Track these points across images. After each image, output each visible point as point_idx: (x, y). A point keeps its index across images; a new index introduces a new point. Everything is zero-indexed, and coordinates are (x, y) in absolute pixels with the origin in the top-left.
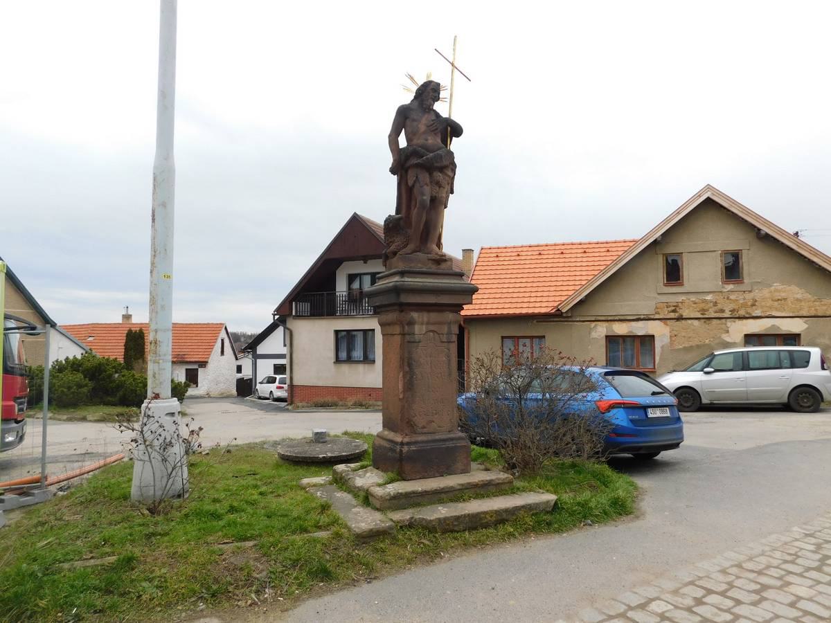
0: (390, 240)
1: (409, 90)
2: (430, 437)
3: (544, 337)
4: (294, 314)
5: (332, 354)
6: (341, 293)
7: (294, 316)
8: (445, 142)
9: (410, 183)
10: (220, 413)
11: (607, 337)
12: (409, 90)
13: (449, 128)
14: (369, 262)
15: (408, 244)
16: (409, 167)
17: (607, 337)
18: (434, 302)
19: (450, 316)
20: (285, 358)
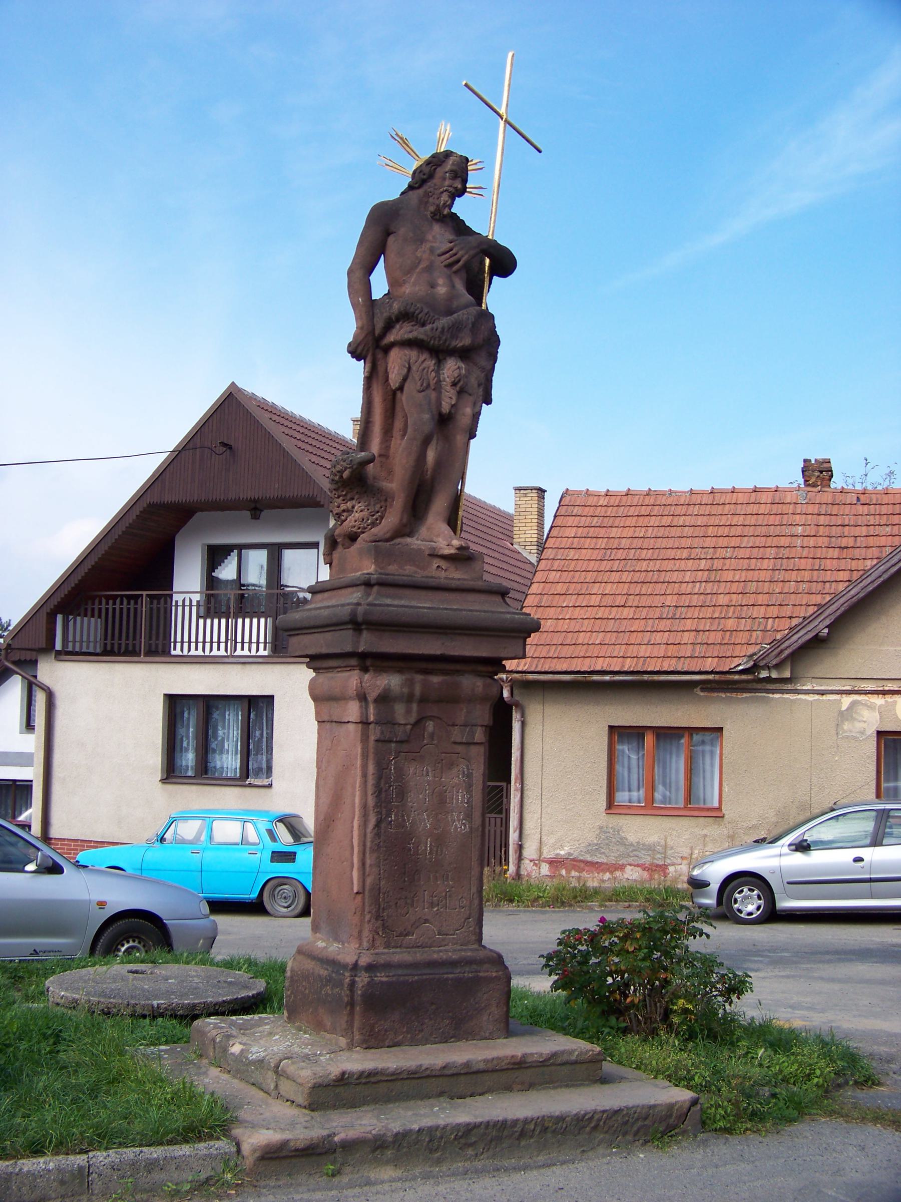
0: (343, 507)
1: (399, 169)
2: (420, 956)
3: (720, 730)
4: (58, 646)
5: (155, 758)
6: (187, 596)
7: (58, 653)
8: (477, 290)
9: (394, 379)
10: (90, 867)
11: (880, 733)
12: (399, 169)
13: (487, 261)
14: (265, 513)
15: (382, 517)
16: (392, 345)
17: (880, 733)
18: (438, 652)
19: (472, 683)
20: (30, 764)
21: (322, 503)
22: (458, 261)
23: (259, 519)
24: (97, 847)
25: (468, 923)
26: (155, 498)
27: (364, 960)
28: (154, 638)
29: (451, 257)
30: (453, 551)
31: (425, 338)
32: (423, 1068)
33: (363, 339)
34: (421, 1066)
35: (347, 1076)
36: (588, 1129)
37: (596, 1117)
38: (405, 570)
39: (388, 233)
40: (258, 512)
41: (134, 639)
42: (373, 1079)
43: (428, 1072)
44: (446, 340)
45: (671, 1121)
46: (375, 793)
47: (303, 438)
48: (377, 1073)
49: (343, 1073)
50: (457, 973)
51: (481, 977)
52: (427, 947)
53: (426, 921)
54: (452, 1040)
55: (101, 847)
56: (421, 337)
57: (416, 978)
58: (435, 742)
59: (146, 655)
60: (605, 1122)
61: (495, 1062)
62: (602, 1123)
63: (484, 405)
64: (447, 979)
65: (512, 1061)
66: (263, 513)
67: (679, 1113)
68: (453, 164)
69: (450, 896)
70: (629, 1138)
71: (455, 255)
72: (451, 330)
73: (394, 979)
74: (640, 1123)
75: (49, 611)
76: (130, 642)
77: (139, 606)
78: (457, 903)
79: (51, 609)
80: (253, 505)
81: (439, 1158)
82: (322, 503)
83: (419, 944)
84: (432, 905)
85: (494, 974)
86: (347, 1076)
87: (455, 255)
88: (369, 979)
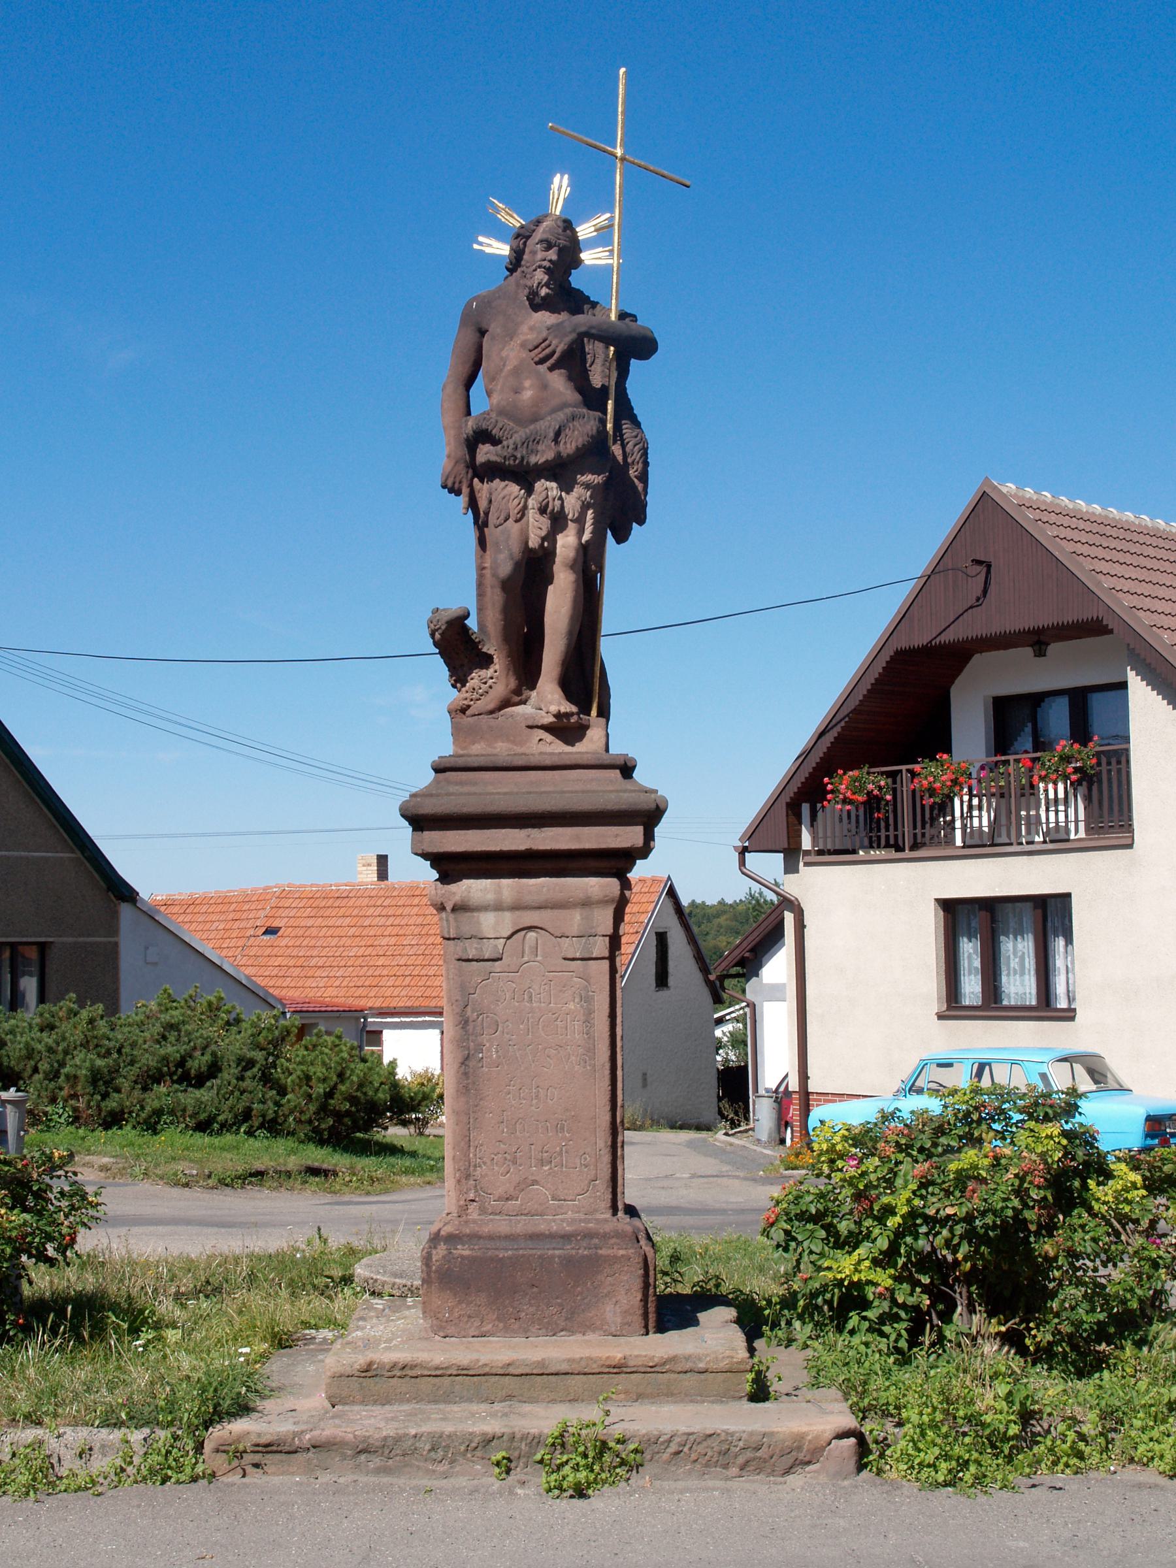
14: (1054, 648)
21: (1110, 627)
22: (554, 353)
23: (1045, 655)
24: (835, 1101)
25: (594, 1186)
26: (905, 641)
27: (1046, 1247)
28: (891, 828)
29: (544, 350)
30: (551, 719)
31: (499, 460)
32: (480, 1364)
33: (452, 470)
34: (478, 1360)
35: (375, 1366)
36: (666, 1456)
37: (677, 1440)
38: (495, 748)
39: (482, 333)
40: (1043, 647)
41: (896, 829)
42: (411, 1373)
43: (487, 1370)
44: (523, 458)
45: (801, 1456)
46: (460, 1023)
47: (1098, 540)
48: (416, 1366)
49: (370, 1364)
50: (569, 1250)
51: (602, 1256)
52: (537, 1215)
53: (535, 1182)
54: (562, 1333)
55: (840, 1101)
56: (494, 458)
57: (510, 1252)
58: (539, 958)
59: (912, 849)
60: (690, 1448)
61: (583, 1363)
62: (686, 1449)
63: (635, 525)
64: (553, 1256)
65: (608, 1363)
66: (1050, 647)
67: (812, 1446)
68: (544, 232)
69: (566, 1152)
70: (734, 1470)
71: (549, 345)
72: (525, 444)
73: (479, 1254)
74: (749, 1454)
75: (788, 800)
76: (891, 833)
77: (898, 786)
78: (578, 1161)
79: (791, 798)
80: (1036, 638)
81: (444, 1473)
82: (1110, 627)
83: (526, 1212)
84: (542, 1163)
85: (621, 1252)
86: (375, 1366)
87: (549, 345)
88: (445, 1252)
